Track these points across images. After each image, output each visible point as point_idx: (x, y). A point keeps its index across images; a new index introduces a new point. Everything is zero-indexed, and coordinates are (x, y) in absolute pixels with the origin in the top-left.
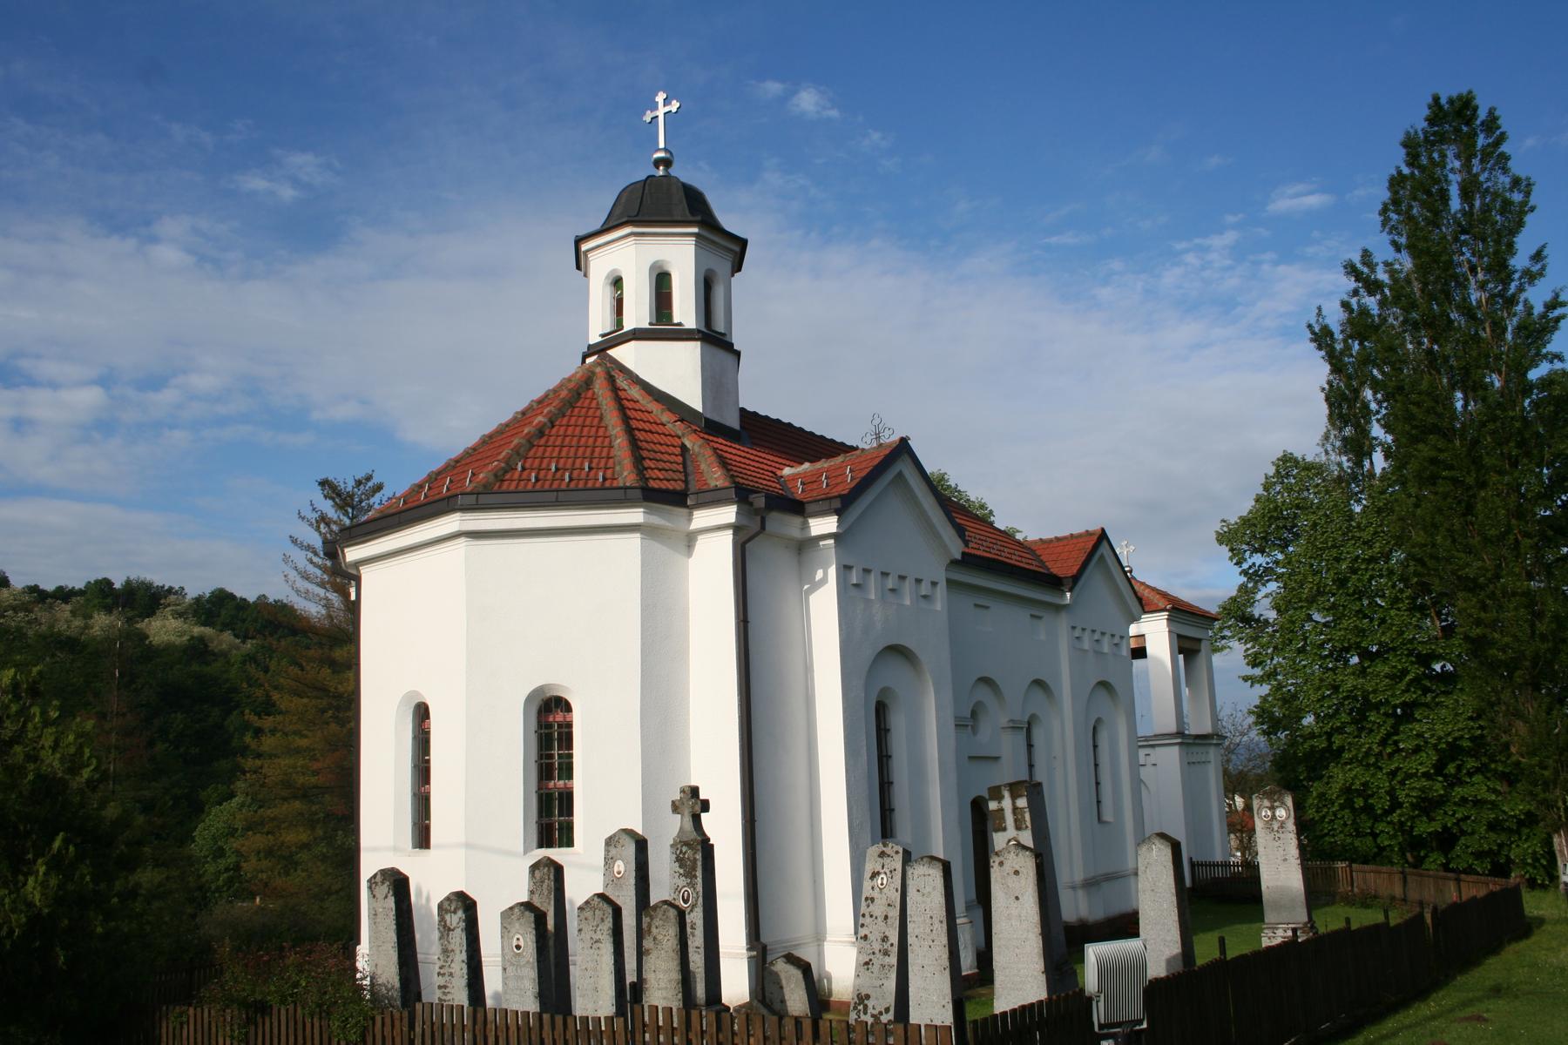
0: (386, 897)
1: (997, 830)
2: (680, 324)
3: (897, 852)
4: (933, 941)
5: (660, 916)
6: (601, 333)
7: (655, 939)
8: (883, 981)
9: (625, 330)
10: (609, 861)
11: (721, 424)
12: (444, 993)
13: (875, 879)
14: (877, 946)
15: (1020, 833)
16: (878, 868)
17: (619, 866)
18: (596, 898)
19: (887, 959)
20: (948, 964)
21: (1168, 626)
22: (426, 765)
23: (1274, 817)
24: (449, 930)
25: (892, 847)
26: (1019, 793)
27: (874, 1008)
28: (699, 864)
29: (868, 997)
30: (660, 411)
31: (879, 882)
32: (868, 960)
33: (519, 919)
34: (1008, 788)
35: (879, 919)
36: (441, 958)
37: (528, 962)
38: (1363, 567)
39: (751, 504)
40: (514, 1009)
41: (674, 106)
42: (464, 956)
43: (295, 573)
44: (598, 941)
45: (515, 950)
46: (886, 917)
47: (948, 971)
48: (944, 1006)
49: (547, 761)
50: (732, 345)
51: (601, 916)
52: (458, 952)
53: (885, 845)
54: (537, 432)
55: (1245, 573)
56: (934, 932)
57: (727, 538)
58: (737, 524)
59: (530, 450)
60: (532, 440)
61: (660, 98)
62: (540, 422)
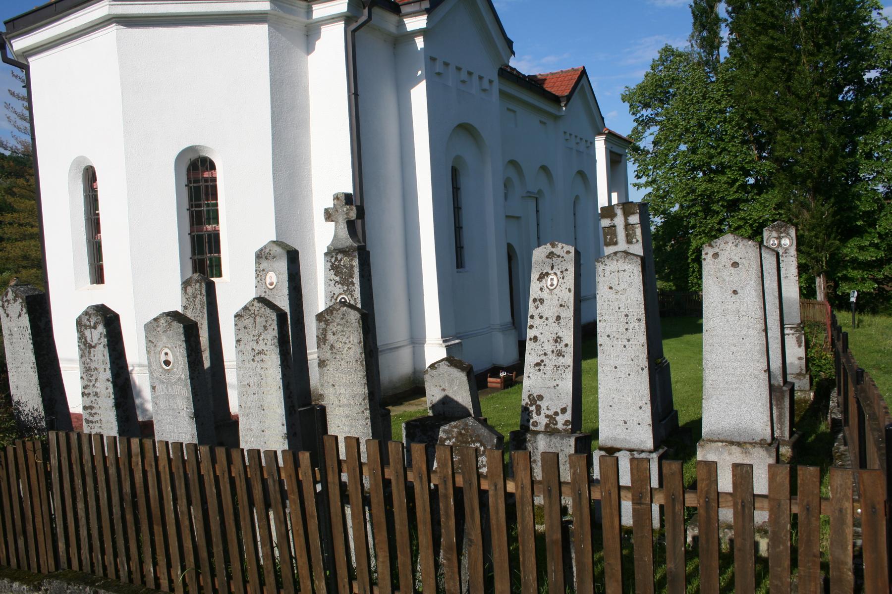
0: (20, 315)
3: (568, 252)
4: (629, 341)
5: (338, 320)
7: (332, 347)
8: (557, 382)
10: (260, 274)
13: (544, 280)
14: (549, 347)
15: (631, 246)
16: (547, 269)
17: (271, 277)
18: (256, 303)
20: (646, 364)
21: (605, 144)
22: (97, 217)
23: (779, 245)
24: (91, 347)
25: (562, 247)
26: (632, 211)
27: (548, 409)
28: (356, 271)
29: (541, 398)
31: (549, 283)
33: (165, 331)
34: (621, 207)
37: (180, 378)
38: (714, 116)
42: (108, 374)
44: (260, 353)
45: (164, 366)
46: (558, 318)
47: (646, 371)
48: (641, 408)
49: (196, 209)
51: (264, 323)
53: (553, 246)
55: (636, 120)
56: (630, 330)
58: (349, 14)
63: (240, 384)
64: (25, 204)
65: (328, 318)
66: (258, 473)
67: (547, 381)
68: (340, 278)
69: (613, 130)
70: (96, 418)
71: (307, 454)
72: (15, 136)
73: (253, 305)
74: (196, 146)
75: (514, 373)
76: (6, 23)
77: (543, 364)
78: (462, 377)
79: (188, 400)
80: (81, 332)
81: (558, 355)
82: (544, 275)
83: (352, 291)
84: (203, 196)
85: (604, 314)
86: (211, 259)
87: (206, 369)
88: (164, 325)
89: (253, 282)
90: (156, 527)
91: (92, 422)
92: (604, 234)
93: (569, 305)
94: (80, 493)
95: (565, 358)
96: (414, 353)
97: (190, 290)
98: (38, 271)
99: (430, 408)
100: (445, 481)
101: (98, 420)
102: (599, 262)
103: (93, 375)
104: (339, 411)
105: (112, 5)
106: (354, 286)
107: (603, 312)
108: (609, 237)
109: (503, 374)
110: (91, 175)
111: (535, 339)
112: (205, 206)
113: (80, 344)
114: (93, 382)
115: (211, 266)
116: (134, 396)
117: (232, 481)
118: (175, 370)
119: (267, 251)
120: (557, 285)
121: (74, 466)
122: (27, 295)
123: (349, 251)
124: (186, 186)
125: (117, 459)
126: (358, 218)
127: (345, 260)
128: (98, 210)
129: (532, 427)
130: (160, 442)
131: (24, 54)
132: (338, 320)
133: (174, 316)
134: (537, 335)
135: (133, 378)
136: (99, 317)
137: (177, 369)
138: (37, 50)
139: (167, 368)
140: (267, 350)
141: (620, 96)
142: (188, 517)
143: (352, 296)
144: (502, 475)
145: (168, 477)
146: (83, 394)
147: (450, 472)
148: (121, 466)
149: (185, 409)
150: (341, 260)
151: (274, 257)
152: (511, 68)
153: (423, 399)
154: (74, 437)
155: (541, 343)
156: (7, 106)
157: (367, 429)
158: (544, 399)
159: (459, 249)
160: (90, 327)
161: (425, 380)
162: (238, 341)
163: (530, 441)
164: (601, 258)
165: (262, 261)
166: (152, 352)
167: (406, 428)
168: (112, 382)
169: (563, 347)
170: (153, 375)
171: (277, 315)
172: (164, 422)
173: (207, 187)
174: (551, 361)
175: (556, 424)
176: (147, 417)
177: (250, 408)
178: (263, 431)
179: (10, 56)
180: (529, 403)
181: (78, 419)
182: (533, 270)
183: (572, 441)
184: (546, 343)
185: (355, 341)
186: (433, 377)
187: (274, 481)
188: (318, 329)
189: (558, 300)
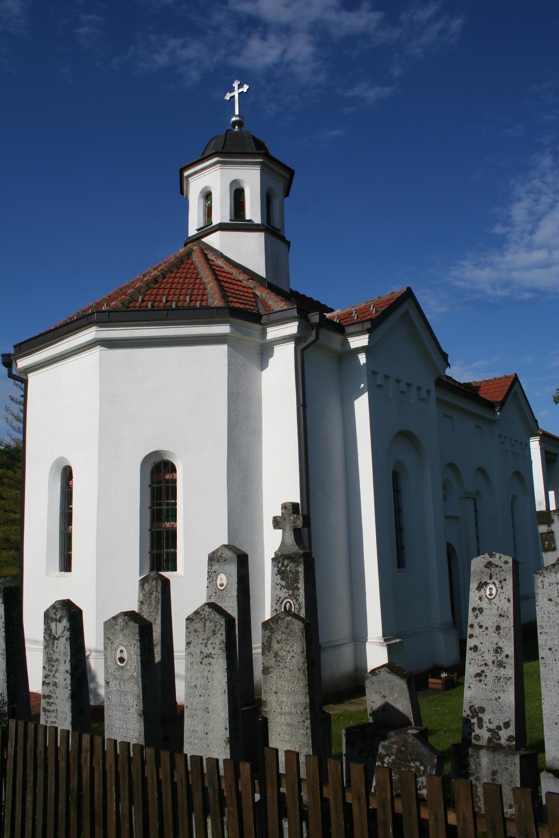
1: (546, 550)
2: (250, 221)
3: (506, 562)
5: (283, 629)
6: (197, 228)
7: (276, 655)
8: (499, 694)
9: (214, 224)
10: (212, 576)
11: (277, 287)
12: (49, 704)
13: (483, 590)
14: (489, 657)
16: (486, 579)
17: (222, 579)
18: (206, 608)
19: (502, 671)
21: (540, 444)
22: (70, 511)
24: (55, 638)
25: (500, 557)
27: (490, 722)
28: (301, 576)
29: (482, 710)
30: (238, 273)
31: (488, 592)
32: (480, 672)
33: (122, 630)
35: (490, 630)
36: (46, 667)
37: (132, 676)
39: (309, 321)
40: (113, 738)
41: (245, 88)
42: (68, 666)
43: (12, 417)
44: (209, 656)
45: (119, 663)
46: (498, 628)
49: (157, 508)
50: (285, 238)
51: (213, 628)
52: (62, 662)
53: (491, 556)
54: (153, 280)
57: (290, 347)
59: (148, 290)
60: (149, 285)
61: (236, 85)
62: (155, 274)
63: (187, 685)
64: (11, 493)
65: (273, 626)
66: (200, 780)
67: (488, 693)
68: (286, 582)
69: (547, 431)
70: (53, 708)
71: (248, 766)
72: (10, 434)
73: (204, 610)
74: (160, 451)
75: (456, 674)
76: (15, 347)
77: (483, 675)
78: (401, 684)
79: (138, 697)
80: (47, 624)
81: (499, 666)
82: (483, 585)
83: (297, 596)
84: (164, 495)
85: (544, 627)
86: (167, 554)
87: (157, 663)
88: (122, 624)
89: (205, 582)
90: (97, 828)
91: (49, 711)
92: (542, 541)
93: (509, 615)
94: (30, 784)
95: (506, 669)
96: (355, 651)
97: (147, 586)
98: (16, 554)
99: (370, 715)
100: (384, 806)
101: (55, 709)
102: (537, 573)
103: (54, 666)
104: (281, 719)
105: (98, 331)
106: (298, 590)
107: (544, 624)
108: (547, 543)
109: (444, 675)
110: (68, 474)
111: (475, 648)
112: (165, 505)
113: (46, 635)
114: (54, 673)
115: (167, 560)
116: (89, 680)
117: (174, 785)
118: (128, 667)
119: (219, 554)
120: (496, 595)
121: (28, 757)
122: (5, 586)
123: (295, 557)
124: (149, 530)
125: (68, 752)
126: (304, 526)
127: (291, 566)
128: (72, 504)
129: (473, 741)
130: (109, 739)
131: (25, 371)
132: (283, 629)
133: (131, 615)
134: (477, 644)
135: (89, 663)
136: (64, 612)
137: (131, 666)
138: (36, 367)
139: (122, 665)
140: (214, 654)
141: (552, 399)
142: (128, 820)
143: (297, 600)
144: (442, 805)
145: (114, 776)
146: (44, 683)
147: (389, 797)
148: (71, 761)
149: (135, 706)
150: (287, 566)
151: (225, 560)
152: (447, 377)
153: (364, 698)
154: (31, 726)
155: (481, 653)
156: (7, 409)
157: (307, 739)
158: (486, 712)
159: (400, 548)
160: (56, 620)
161: (366, 685)
162: (188, 643)
163: (472, 756)
164: (539, 570)
165: (213, 563)
166: (109, 649)
167: (346, 735)
168: (70, 674)
169: (504, 658)
170: (108, 671)
171: (226, 621)
172: (115, 717)
173: (167, 488)
174: (492, 672)
175: (499, 739)
176: (99, 702)
177: (196, 709)
178: (207, 734)
179: (14, 372)
180: (471, 715)
181: (36, 698)
182: (471, 579)
183: (517, 760)
184: (486, 653)
185: (299, 650)
186: (373, 683)
187: (214, 790)
188: (263, 636)
189: (498, 610)
